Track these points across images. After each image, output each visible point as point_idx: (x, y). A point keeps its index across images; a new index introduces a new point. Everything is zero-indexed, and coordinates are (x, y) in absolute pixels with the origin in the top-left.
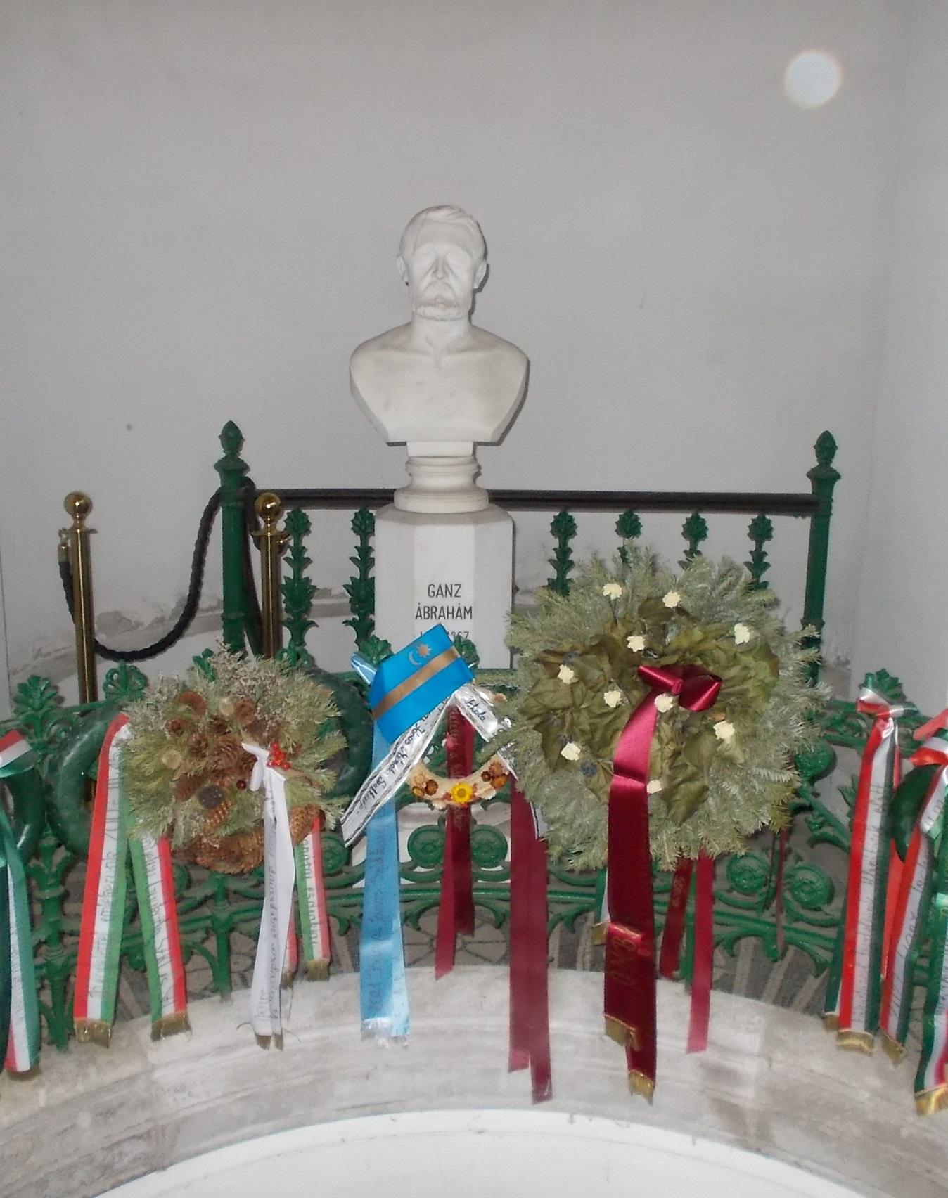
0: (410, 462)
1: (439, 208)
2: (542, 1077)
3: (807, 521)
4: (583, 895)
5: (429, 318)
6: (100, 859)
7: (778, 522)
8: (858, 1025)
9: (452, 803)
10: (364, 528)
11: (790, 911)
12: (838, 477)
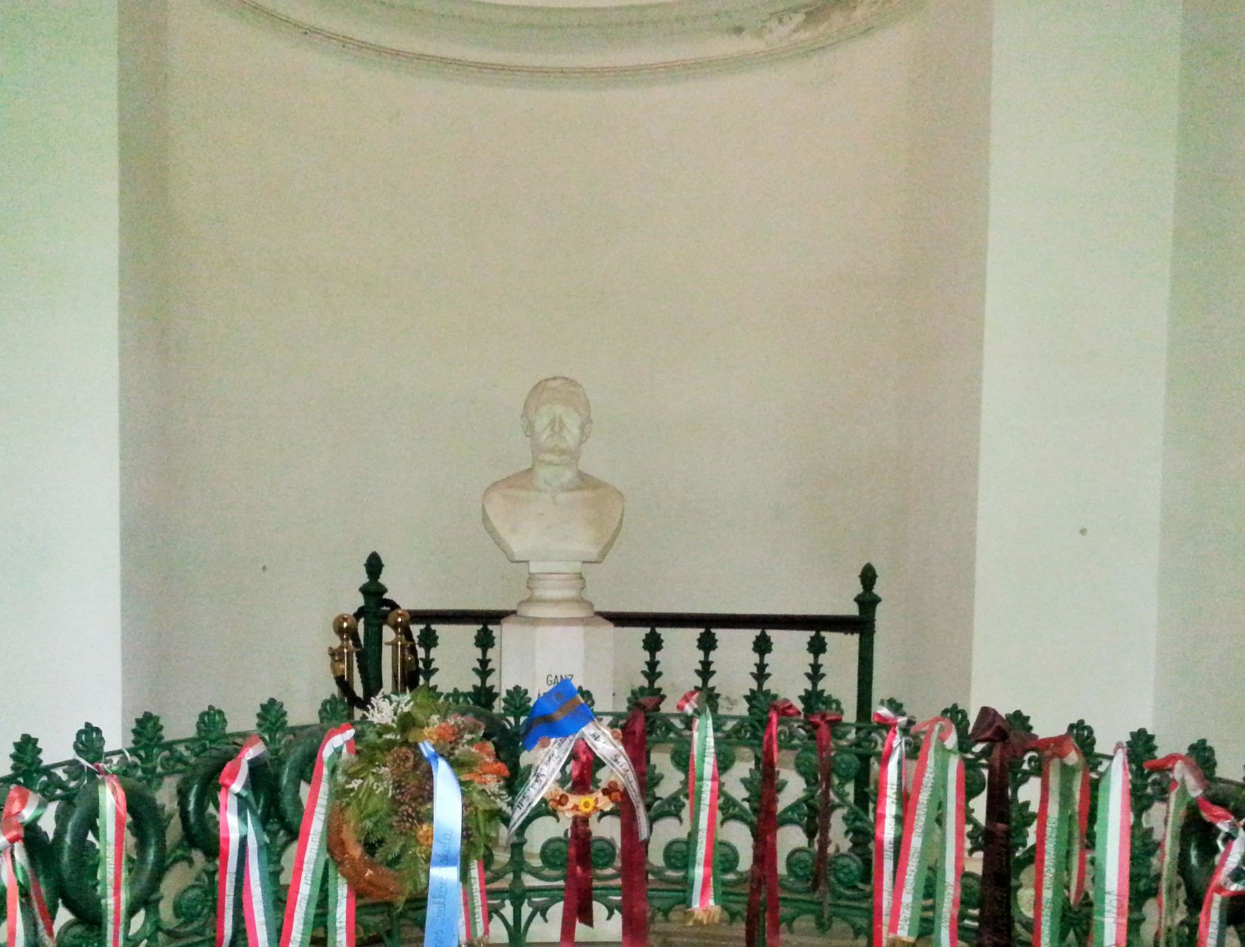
0: (532, 577)
1: (555, 378)
3: (856, 637)
4: (675, 891)
6: (308, 834)
7: (830, 637)
9: (579, 813)
10: (485, 641)
11: (833, 892)
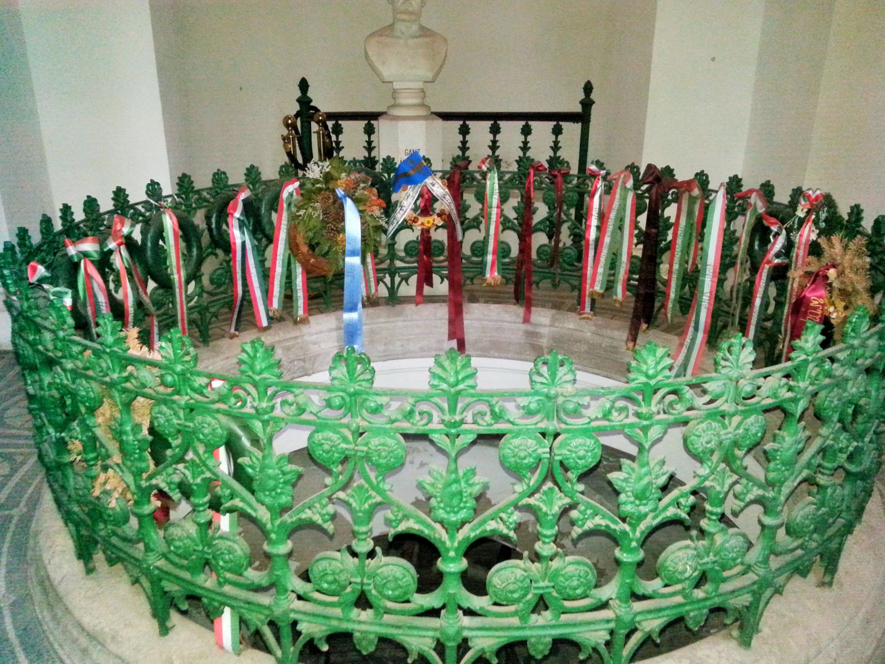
0: (395, 92)
2: (461, 346)
5: (404, 21)
7: (565, 125)
8: (588, 309)
10: (369, 130)
12: (594, 103)
